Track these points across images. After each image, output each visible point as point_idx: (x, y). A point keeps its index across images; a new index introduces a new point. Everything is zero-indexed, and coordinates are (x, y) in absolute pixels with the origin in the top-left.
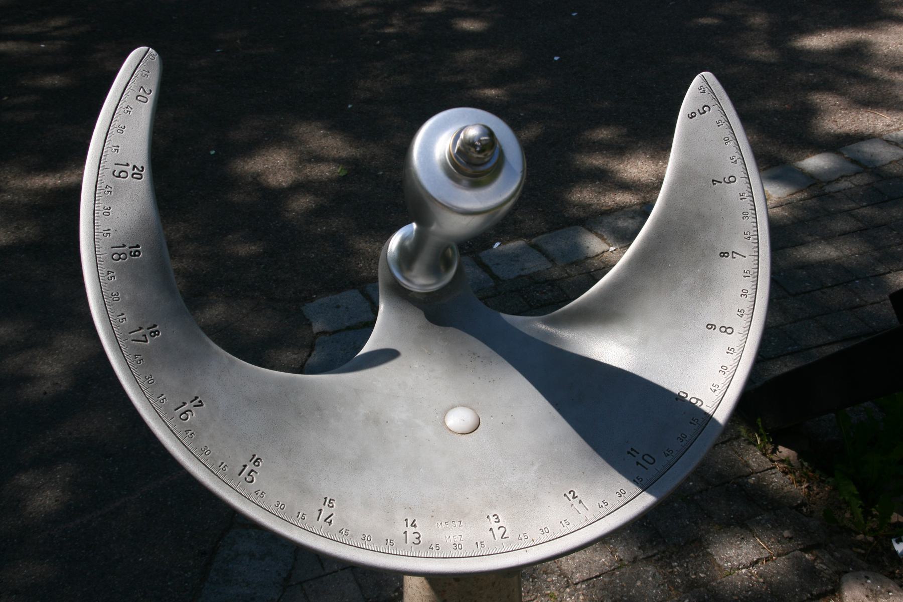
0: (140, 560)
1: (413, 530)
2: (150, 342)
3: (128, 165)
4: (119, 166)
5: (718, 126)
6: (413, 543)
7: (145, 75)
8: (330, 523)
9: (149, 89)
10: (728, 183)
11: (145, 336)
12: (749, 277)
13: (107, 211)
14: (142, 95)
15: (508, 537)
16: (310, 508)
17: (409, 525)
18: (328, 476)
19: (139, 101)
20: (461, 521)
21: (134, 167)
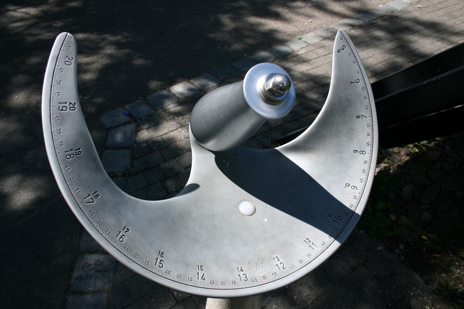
1: (242, 273)
2: (96, 202)
4: (61, 104)
5: (350, 55)
6: (245, 280)
7: (68, 49)
8: (204, 279)
9: (71, 57)
11: (92, 199)
12: (369, 127)
13: (59, 131)
14: (68, 61)
16: (192, 273)
18: (196, 253)
19: (67, 64)
20: (262, 264)
21: (70, 103)
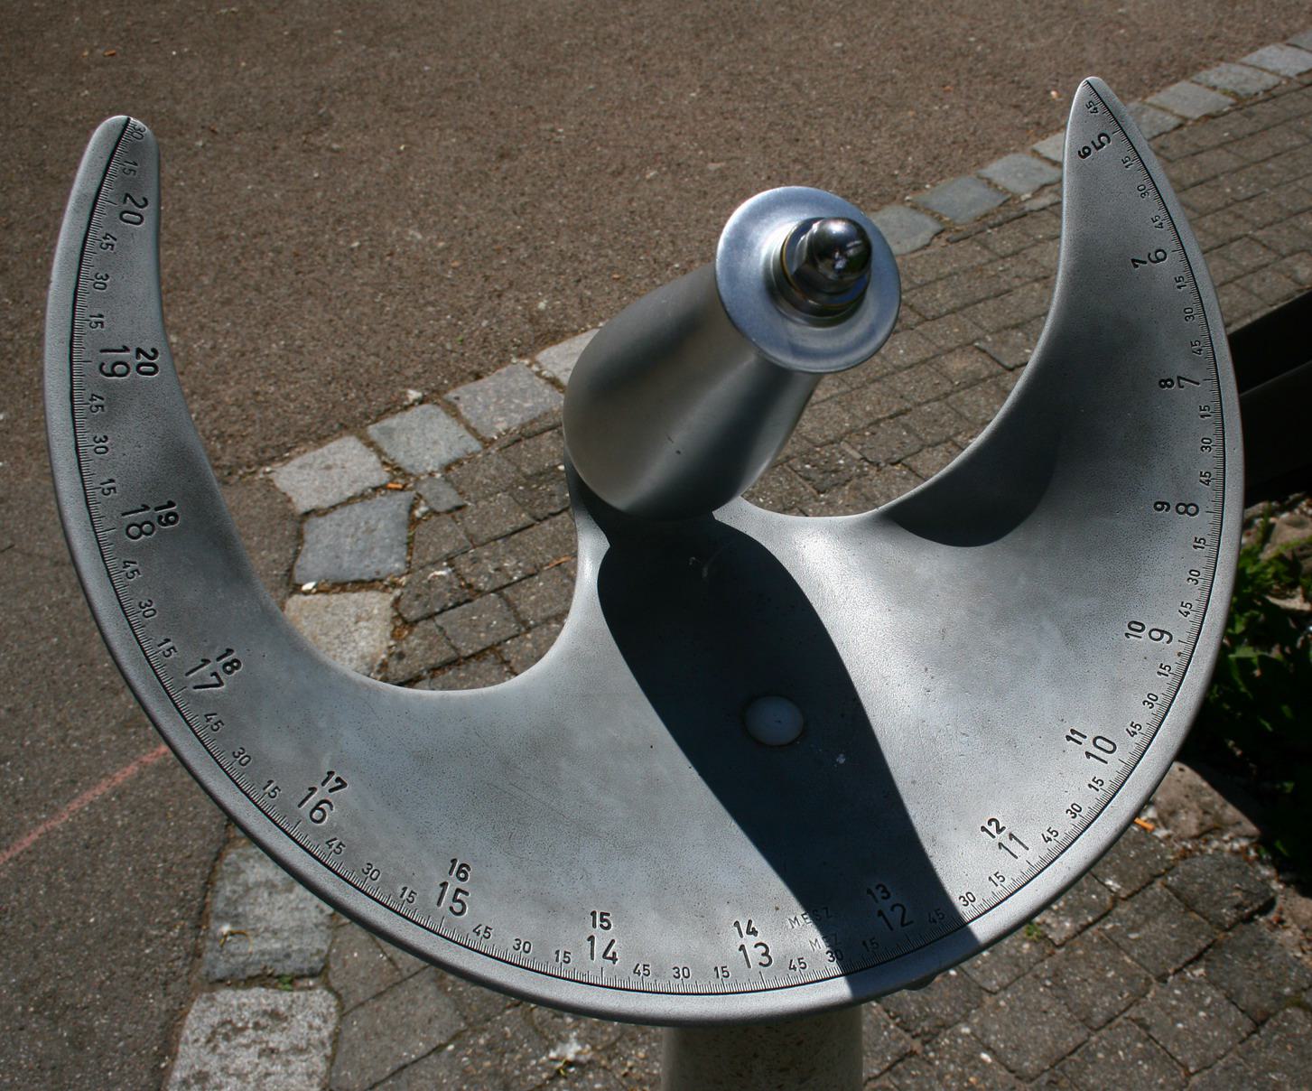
0: (92, 920)
3: (126, 349)
10: (1155, 262)
15: (912, 922)
17: (744, 932)
